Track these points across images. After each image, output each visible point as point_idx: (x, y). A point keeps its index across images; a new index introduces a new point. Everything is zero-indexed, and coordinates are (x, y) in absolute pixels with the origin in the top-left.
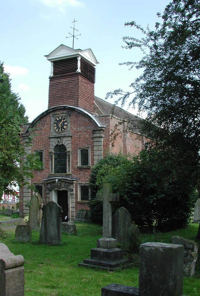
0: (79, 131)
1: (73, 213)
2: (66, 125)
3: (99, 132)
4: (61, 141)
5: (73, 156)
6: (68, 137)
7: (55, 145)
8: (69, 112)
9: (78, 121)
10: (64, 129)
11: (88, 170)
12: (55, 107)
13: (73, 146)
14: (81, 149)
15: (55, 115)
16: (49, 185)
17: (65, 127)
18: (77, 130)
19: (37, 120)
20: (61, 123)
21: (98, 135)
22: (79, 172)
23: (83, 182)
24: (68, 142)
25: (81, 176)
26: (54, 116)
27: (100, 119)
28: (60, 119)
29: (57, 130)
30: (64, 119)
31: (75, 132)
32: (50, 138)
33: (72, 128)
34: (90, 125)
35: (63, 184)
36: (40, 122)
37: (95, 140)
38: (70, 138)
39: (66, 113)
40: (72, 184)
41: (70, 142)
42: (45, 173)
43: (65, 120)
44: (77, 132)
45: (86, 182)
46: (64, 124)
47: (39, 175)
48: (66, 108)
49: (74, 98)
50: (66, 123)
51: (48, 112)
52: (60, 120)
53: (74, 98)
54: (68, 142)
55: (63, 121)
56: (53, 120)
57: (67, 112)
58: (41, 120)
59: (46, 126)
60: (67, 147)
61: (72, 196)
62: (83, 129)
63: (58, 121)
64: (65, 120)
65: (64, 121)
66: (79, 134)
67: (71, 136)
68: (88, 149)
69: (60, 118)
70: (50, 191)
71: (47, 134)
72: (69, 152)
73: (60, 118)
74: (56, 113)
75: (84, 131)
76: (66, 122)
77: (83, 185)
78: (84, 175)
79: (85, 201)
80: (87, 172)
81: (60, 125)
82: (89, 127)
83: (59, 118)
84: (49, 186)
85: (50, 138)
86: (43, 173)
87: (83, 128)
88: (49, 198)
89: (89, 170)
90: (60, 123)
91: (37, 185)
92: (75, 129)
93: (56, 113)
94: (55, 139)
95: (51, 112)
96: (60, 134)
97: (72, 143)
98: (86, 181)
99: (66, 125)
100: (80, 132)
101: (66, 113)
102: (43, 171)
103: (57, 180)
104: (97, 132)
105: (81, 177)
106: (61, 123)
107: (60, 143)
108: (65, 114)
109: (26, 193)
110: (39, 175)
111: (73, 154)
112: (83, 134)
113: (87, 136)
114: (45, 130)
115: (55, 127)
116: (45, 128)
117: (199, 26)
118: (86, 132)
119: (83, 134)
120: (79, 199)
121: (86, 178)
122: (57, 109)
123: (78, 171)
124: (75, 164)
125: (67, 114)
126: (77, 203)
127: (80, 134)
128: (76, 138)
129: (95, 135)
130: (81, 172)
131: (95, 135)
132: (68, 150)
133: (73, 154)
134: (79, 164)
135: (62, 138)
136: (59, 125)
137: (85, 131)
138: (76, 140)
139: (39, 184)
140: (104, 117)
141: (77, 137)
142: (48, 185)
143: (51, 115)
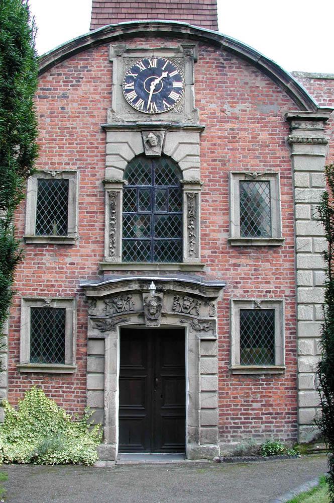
0: (230, 115)
1: (211, 411)
2: (178, 90)
3: (309, 127)
4: (159, 141)
5: (207, 201)
6: (187, 129)
7: (130, 156)
8: (189, 47)
9: (225, 82)
10: (172, 102)
11: (271, 252)
12: (138, 21)
13: (205, 165)
14: (243, 178)
15: (128, 51)
16: (101, 306)
17: (173, 95)
18: (223, 111)
19: (53, 60)
20: (157, 81)
21: (313, 136)
22: (232, 261)
23: (253, 296)
24: (188, 149)
25: (243, 276)
26: (126, 55)
27: (311, 85)
28: (151, 69)
29: (140, 104)
30: (170, 69)
31: (214, 117)
32: (105, 130)
33: (203, 102)
34: (276, 103)
35: (168, 303)
36: (61, 71)
37: (298, 149)
38: (195, 137)
39: (177, 50)
40: (206, 304)
41: (196, 150)
42: (80, 261)
43: (175, 73)
44: (223, 117)
45: (265, 296)
46: (171, 84)
47: (48, 269)
48: (184, 31)
49: (200, 12)
50: (176, 85)
51: (104, 37)
52: (155, 72)
53: (200, 12)
54: (188, 149)
55: (165, 75)
56: (119, 69)
57: (181, 48)
58: (66, 63)
59: (85, 88)
60: (182, 166)
61: (207, 350)
62: (245, 111)
63: (142, 75)
64: (175, 73)
65: (171, 75)
66: (230, 125)
67: (201, 130)
68: (270, 179)
69: (154, 65)
70: (103, 331)
71: (94, 117)
72: (197, 183)
73: (154, 65)
74: (133, 46)
75: (249, 119)
76: (178, 78)
77: (252, 307)
78: (255, 270)
79: (265, 367)
80: (268, 261)
81: (152, 88)
82: (272, 107)
83: (146, 63)
84: (99, 310)
85: (105, 130)
86: (68, 260)
87: (247, 106)
88: (102, 356)
89: (275, 252)
90: (153, 80)
91: (39, 305)
92: (213, 106)
93: (133, 46)
94: (131, 134)
95: (115, 39)
96: (154, 118)
97: (202, 155)
98: (261, 292)
99: (178, 90)
100: (236, 118)
101: (177, 50)
102: (70, 251)
103: (153, 286)
104: (303, 125)
105: (244, 278)
106: (157, 81)
107: (156, 149)
108: (172, 55)
109: (310, 238)
110: (48, 265)
111: (207, 194)
112: (246, 126)
113: (264, 136)
114: (83, 99)
115: (128, 91)
116: (80, 92)
117: (1, 72)
118: (260, 121)
119: (246, 126)
120: (235, 362)
121: (261, 283)
122: (141, 30)
123: (233, 257)
124: (214, 231)
125: (180, 55)
126: (228, 373)
127: (237, 126)
128: (219, 137)
129: (297, 134)
130: (243, 260)
131: (297, 134)
132: (187, 176)
133: (207, 194)
134: (236, 232)
135: (163, 133)
136: (149, 85)
137: (253, 119)
138: (219, 145)
139: (53, 300)
140: (323, 82)
141: (226, 137)
142: (95, 305)
143: (112, 49)
